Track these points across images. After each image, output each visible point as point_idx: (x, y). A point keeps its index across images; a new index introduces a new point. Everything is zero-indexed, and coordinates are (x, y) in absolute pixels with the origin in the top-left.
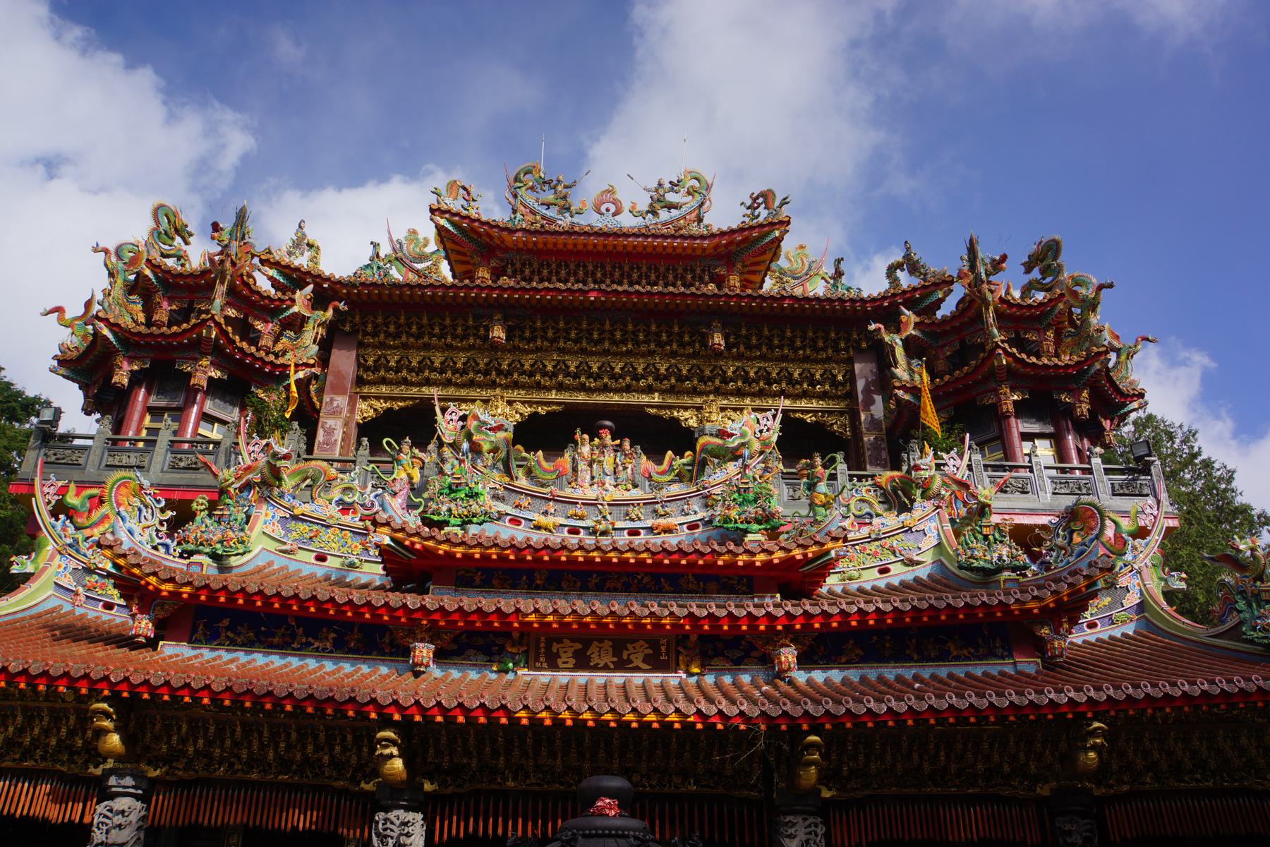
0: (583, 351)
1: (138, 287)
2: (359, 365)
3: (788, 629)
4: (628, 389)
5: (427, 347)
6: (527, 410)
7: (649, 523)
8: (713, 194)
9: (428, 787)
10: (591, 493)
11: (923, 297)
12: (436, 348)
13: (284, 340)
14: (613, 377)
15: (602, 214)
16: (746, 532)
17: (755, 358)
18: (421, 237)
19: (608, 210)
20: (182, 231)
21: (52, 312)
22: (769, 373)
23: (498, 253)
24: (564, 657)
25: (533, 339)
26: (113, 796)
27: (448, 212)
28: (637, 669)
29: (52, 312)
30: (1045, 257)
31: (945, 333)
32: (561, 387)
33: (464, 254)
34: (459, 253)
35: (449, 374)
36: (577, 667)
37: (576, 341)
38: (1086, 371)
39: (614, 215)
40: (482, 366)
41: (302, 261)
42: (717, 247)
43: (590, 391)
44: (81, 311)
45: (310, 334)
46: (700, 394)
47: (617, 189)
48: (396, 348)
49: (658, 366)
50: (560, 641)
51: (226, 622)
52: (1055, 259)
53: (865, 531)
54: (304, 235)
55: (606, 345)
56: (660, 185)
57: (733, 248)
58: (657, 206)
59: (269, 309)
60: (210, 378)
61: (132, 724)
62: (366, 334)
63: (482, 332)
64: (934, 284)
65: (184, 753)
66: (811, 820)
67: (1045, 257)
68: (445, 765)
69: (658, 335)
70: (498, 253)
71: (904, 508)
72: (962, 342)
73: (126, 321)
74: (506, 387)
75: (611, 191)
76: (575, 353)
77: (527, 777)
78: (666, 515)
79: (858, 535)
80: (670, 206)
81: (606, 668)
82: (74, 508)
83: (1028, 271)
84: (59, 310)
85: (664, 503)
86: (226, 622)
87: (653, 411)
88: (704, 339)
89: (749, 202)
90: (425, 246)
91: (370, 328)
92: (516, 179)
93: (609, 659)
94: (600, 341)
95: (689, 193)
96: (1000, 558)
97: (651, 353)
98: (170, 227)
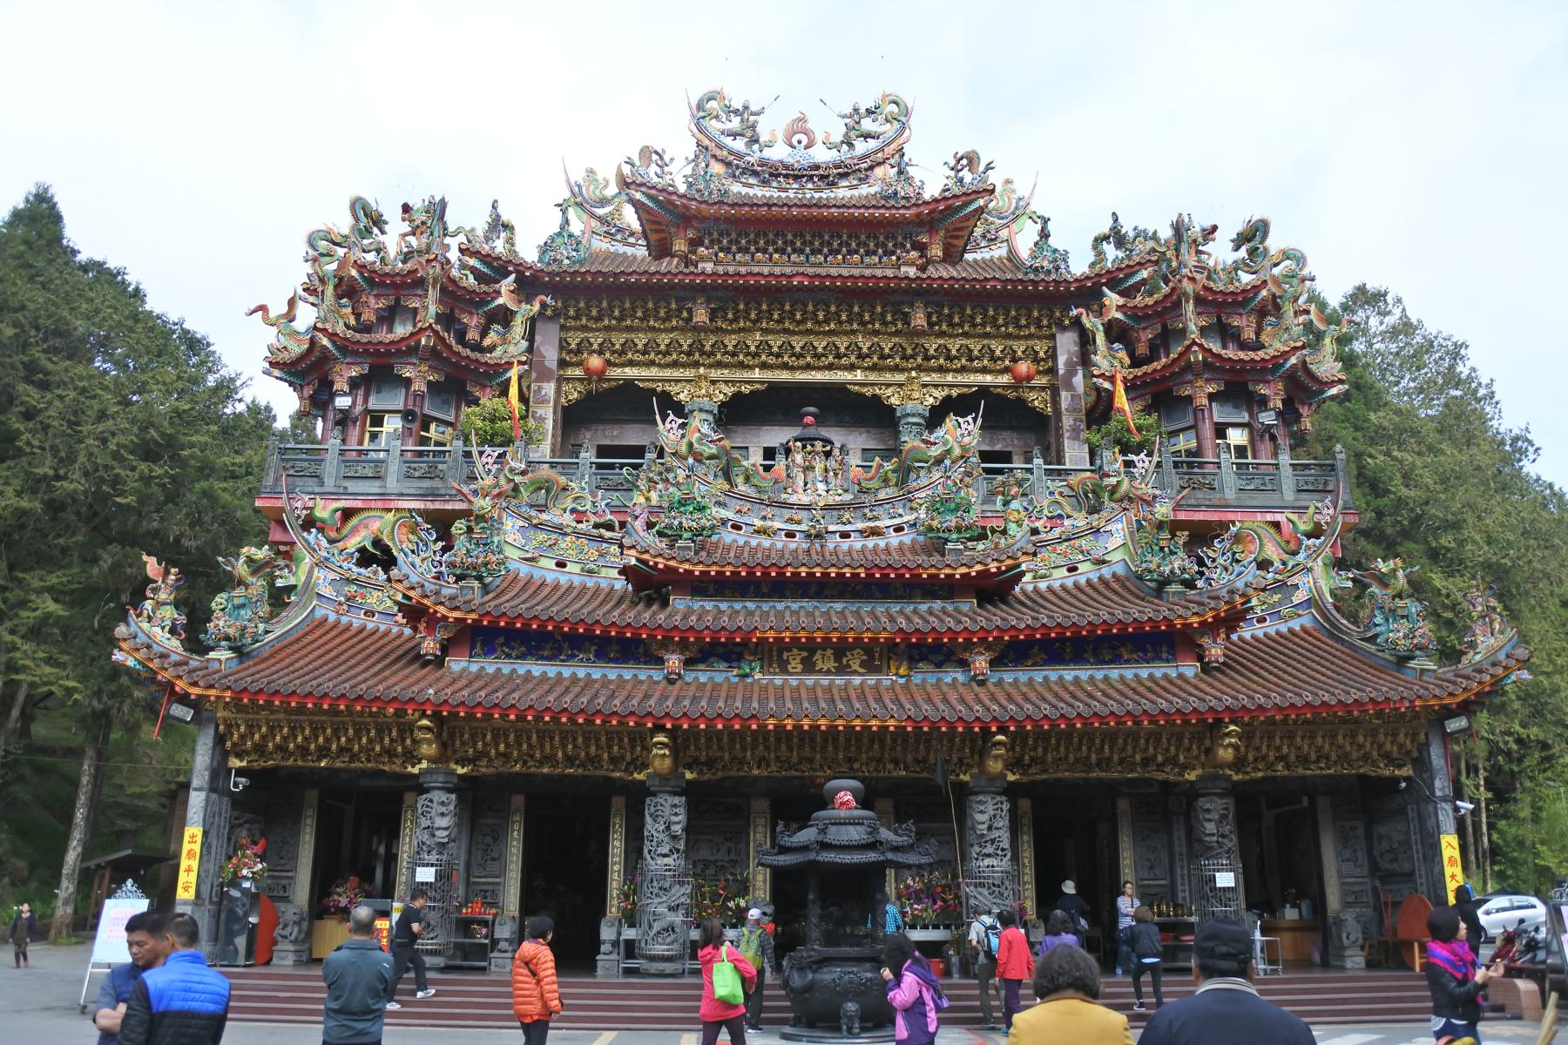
0: (786, 331)
1: (347, 290)
2: (561, 348)
3: (983, 640)
4: (830, 367)
5: (629, 329)
6: (729, 390)
7: (860, 525)
8: (913, 122)
9: (689, 776)
10: (805, 500)
11: (1128, 276)
12: (638, 330)
13: (492, 333)
14: (817, 356)
15: (793, 147)
16: (947, 540)
17: (958, 335)
18: (600, 177)
20: (378, 221)
22: (971, 351)
23: (695, 223)
24: (793, 664)
25: (736, 320)
26: (427, 791)
27: (643, 185)
28: (855, 672)
30: (1252, 236)
31: (1147, 316)
33: (659, 223)
34: (654, 222)
36: (804, 671)
37: (778, 322)
38: (1282, 365)
40: (685, 347)
41: (499, 246)
42: (919, 215)
43: (792, 369)
44: (285, 309)
45: (518, 328)
46: (903, 370)
47: (809, 116)
48: (598, 330)
50: (789, 650)
51: (502, 640)
52: (1263, 241)
53: (1056, 532)
54: (498, 216)
55: (809, 325)
56: (856, 110)
57: (936, 215)
58: (853, 134)
59: (474, 301)
60: (429, 382)
61: (445, 734)
63: (685, 314)
64: (1139, 264)
65: (487, 755)
66: (998, 798)
67: (1252, 236)
68: (703, 759)
69: (861, 315)
70: (695, 223)
71: (1093, 510)
72: (1164, 326)
73: (340, 329)
74: (711, 366)
75: (802, 119)
76: (778, 332)
77: (768, 765)
78: (876, 518)
79: (1050, 536)
80: (867, 136)
81: (828, 672)
82: (323, 521)
83: (1237, 249)
84: (262, 308)
85: (872, 507)
86: (502, 640)
88: (906, 319)
89: (952, 162)
90: (606, 186)
91: (572, 313)
92: (700, 107)
93: (831, 664)
94: (803, 321)
95: (887, 121)
96: (1172, 572)
97: (853, 332)
98: (368, 219)
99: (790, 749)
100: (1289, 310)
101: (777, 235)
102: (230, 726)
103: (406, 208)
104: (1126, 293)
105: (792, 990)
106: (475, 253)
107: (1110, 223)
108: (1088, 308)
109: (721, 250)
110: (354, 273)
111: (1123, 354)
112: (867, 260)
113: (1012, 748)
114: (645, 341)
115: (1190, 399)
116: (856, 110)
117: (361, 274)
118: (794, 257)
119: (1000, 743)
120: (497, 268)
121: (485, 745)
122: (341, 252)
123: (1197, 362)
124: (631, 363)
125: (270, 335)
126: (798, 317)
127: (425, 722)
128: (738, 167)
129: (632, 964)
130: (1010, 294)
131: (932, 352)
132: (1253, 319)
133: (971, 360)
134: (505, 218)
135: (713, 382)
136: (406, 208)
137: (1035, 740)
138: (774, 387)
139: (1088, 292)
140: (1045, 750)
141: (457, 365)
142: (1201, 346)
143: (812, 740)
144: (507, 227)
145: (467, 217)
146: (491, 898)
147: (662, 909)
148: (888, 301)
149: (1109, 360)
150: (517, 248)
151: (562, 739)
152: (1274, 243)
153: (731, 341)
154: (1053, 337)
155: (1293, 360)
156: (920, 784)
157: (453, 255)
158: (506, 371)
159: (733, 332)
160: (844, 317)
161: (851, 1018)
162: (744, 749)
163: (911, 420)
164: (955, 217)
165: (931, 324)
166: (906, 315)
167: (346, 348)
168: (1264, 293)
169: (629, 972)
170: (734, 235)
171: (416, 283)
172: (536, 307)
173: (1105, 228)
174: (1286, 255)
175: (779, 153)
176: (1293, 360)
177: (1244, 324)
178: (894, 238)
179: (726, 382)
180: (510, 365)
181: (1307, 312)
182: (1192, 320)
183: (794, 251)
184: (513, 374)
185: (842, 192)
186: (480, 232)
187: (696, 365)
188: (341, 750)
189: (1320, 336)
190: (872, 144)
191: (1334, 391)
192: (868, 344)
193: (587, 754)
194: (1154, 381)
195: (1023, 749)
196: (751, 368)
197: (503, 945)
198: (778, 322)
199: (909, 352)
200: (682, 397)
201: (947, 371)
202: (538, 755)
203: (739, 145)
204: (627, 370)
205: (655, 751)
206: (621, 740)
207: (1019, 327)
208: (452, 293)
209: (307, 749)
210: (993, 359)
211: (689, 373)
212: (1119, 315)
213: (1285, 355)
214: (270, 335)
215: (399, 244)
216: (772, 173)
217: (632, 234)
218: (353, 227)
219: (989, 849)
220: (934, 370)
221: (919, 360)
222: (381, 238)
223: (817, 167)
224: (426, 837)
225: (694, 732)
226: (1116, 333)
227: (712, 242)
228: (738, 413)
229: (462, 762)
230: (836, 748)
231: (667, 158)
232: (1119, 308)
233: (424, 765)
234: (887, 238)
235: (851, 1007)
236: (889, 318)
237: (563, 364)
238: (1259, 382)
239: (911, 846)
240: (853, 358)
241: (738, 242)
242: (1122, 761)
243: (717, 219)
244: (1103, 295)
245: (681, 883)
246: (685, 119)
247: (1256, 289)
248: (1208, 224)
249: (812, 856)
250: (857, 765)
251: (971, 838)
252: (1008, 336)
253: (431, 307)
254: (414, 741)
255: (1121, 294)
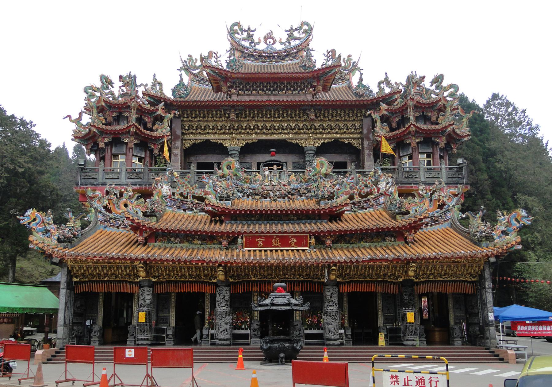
0: (264, 121)
1: (101, 110)
2: (182, 128)
4: (280, 133)
5: (207, 121)
6: (244, 143)
8: (314, 32)
9: (231, 280)
11: (389, 98)
13: (156, 125)
18: (194, 58)
19: (270, 42)
20: (110, 83)
21: (67, 117)
23: (230, 80)
26: (143, 287)
29: (67, 117)
30: (438, 80)
32: (256, 133)
33: (216, 80)
34: (214, 80)
35: (216, 130)
39: (272, 44)
43: (267, 134)
44: (78, 116)
45: (166, 122)
46: (307, 134)
49: (291, 125)
54: (156, 80)
56: (292, 28)
57: (320, 75)
59: (150, 113)
62: (184, 117)
63: (227, 115)
67: (438, 80)
68: (235, 275)
70: (230, 80)
73: (100, 125)
75: (271, 33)
76: (261, 121)
77: (257, 277)
80: (296, 39)
84: (69, 116)
87: (290, 141)
89: (326, 54)
91: (185, 116)
94: (270, 117)
98: (106, 81)
99: (264, 271)
100: (448, 109)
101: (260, 84)
102: (73, 268)
103: (121, 77)
104: (389, 104)
105: (264, 349)
106: (149, 95)
107: (385, 76)
108: (375, 110)
109: (240, 90)
110: (103, 104)
111: (387, 127)
112: (294, 92)
113: (339, 270)
114: (213, 125)
115: (410, 144)
116: (292, 28)
117: (106, 104)
118: (267, 92)
119: (334, 269)
120: (155, 100)
121: (162, 271)
122: (98, 94)
123: (413, 131)
124: (208, 133)
125: (74, 126)
126: (268, 116)
127: (141, 265)
128: (246, 53)
129: (213, 341)
130: (346, 105)
131: (317, 127)
132: (436, 113)
133: (332, 129)
134: (158, 80)
135: (238, 140)
136: (121, 77)
137: (346, 268)
138: (260, 141)
139: (374, 104)
140: (350, 271)
141: (144, 137)
142: (414, 125)
143: (272, 268)
144: (160, 84)
145: (144, 80)
146: (166, 321)
147: (223, 324)
148: (301, 109)
149: (382, 130)
150: (164, 92)
151: (188, 269)
152: (445, 84)
153: (244, 125)
154: (362, 120)
155: (449, 129)
156: (308, 284)
157: (140, 95)
158: (162, 139)
159: (245, 121)
160: (285, 116)
161: (282, 358)
162: (249, 271)
163: (310, 152)
164: (326, 76)
165: (317, 117)
166: (308, 114)
167: (103, 132)
168: (440, 103)
169: (212, 344)
170: (244, 84)
171: (126, 107)
172: (172, 115)
173: (382, 78)
174: (451, 86)
175: (262, 47)
176: (449, 129)
177: (433, 116)
178: (304, 84)
179: (243, 139)
180: (163, 137)
181: (457, 109)
182: (411, 115)
183: (267, 90)
184: (165, 140)
185: (286, 62)
186: (149, 86)
187: (232, 133)
188: (112, 274)
189: (461, 118)
190: (297, 42)
191: (466, 139)
192: (294, 125)
193: (196, 274)
194: (397, 138)
195: (342, 271)
196: (252, 134)
197: (170, 336)
198: (261, 117)
199: (309, 127)
200: (227, 145)
201: (323, 133)
202: (180, 275)
203: (246, 44)
204: (206, 135)
205: (219, 273)
206: (208, 269)
207: (349, 117)
208: (141, 110)
209: (100, 274)
210: (340, 129)
211: (229, 137)
212: (386, 113)
213: (446, 127)
214: (74, 126)
215: (119, 91)
216: (260, 56)
217: (207, 81)
218: (101, 86)
219: (331, 304)
220: (318, 133)
221: (313, 130)
222: (112, 89)
223: (277, 53)
224: (143, 302)
225: (231, 267)
226: (384, 119)
227: (236, 87)
228: (247, 150)
229: (154, 277)
230: (280, 271)
231: (218, 55)
232: (386, 110)
233: (141, 278)
234: (301, 84)
235: (282, 355)
236: (301, 115)
237: (183, 134)
238: (436, 137)
239: (301, 304)
240: (289, 130)
241: (246, 87)
242: (376, 275)
243: (238, 78)
244: (380, 105)
245: (229, 315)
246: (225, 34)
247: (438, 102)
248: (422, 75)
249: (269, 308)
250: (287, 276)
251: (325, 300)
252: (345, 120)
253: (134, 116)
254: (137, 271)
255: (387, 104)
